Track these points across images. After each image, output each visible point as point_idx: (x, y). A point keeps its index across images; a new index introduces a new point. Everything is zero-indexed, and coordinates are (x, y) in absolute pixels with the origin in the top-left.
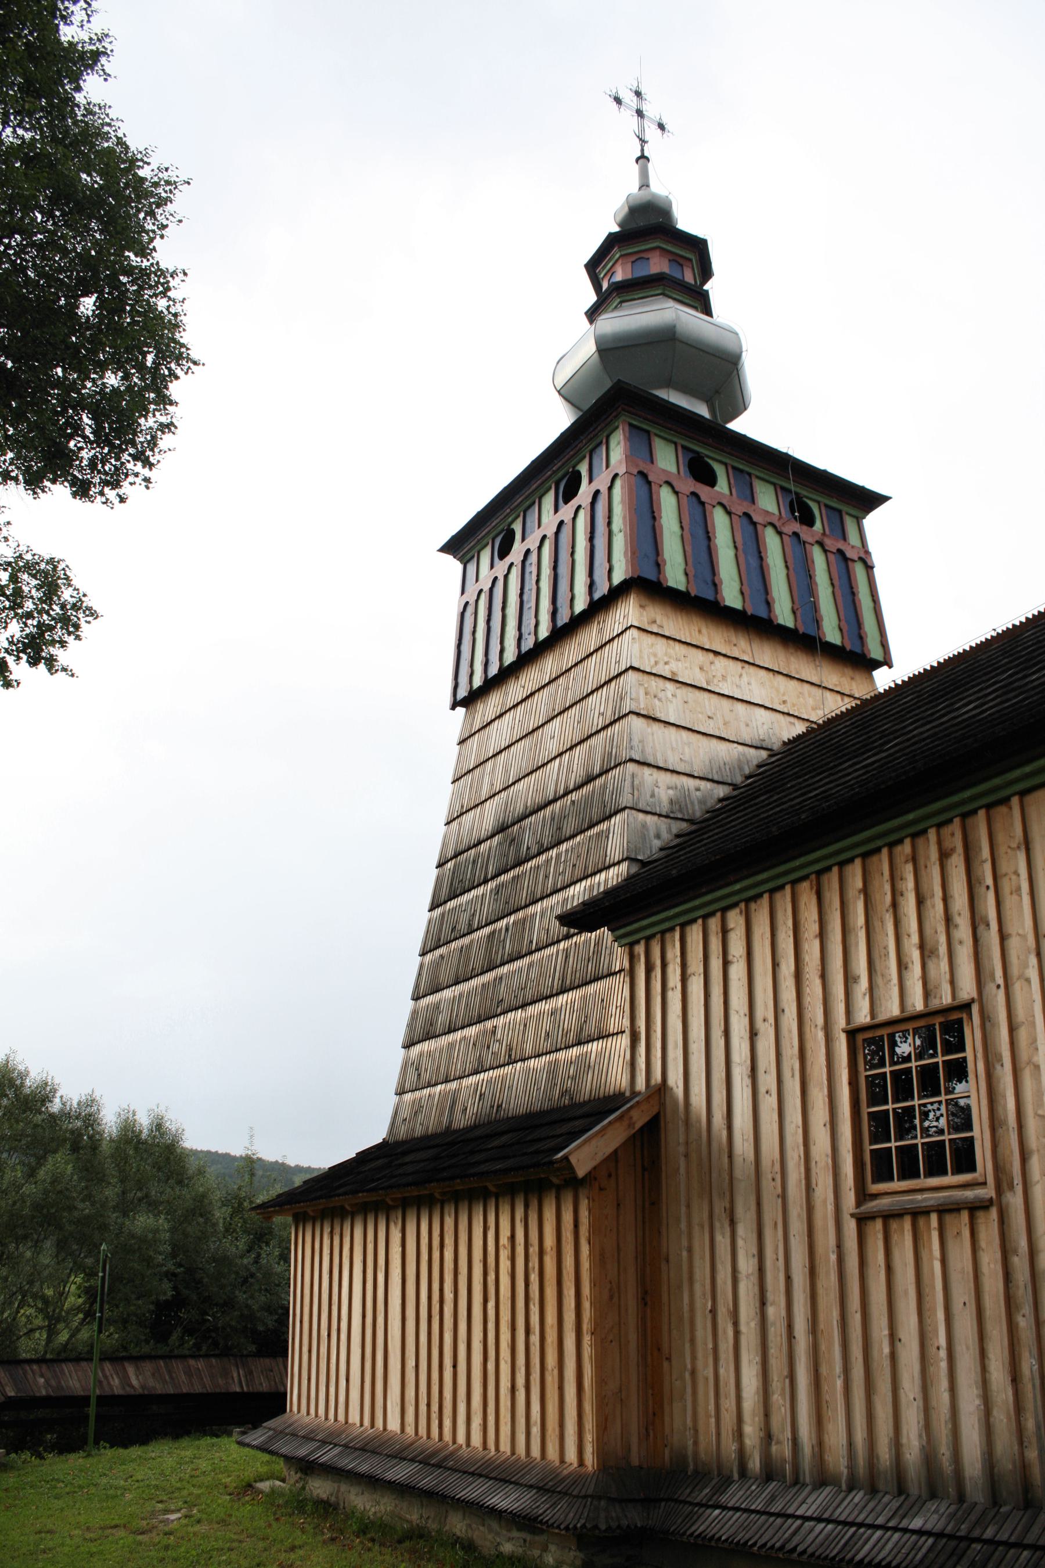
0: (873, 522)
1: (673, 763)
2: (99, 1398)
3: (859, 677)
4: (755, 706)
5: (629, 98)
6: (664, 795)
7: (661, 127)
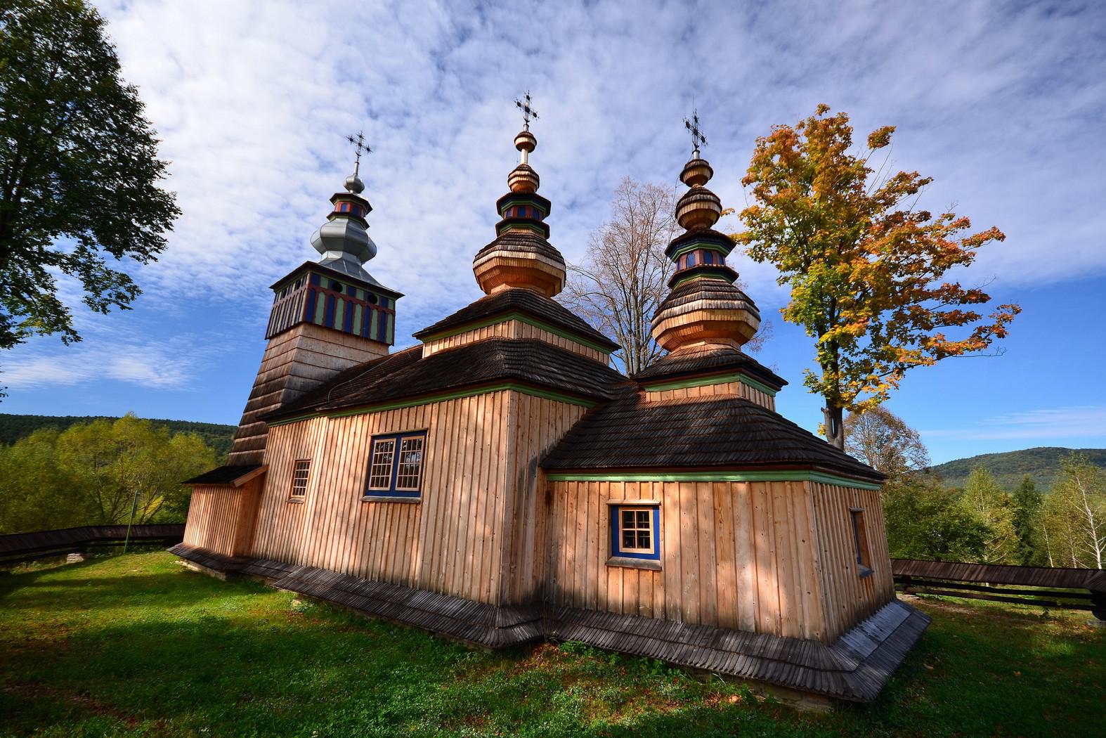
0: (398, 302)
1: (304, 375)
2: (132, 526)
3: (383, 348)
4: (344, 355)
5: (357, 139)
6: (299, 384)
7: (368, 149)
